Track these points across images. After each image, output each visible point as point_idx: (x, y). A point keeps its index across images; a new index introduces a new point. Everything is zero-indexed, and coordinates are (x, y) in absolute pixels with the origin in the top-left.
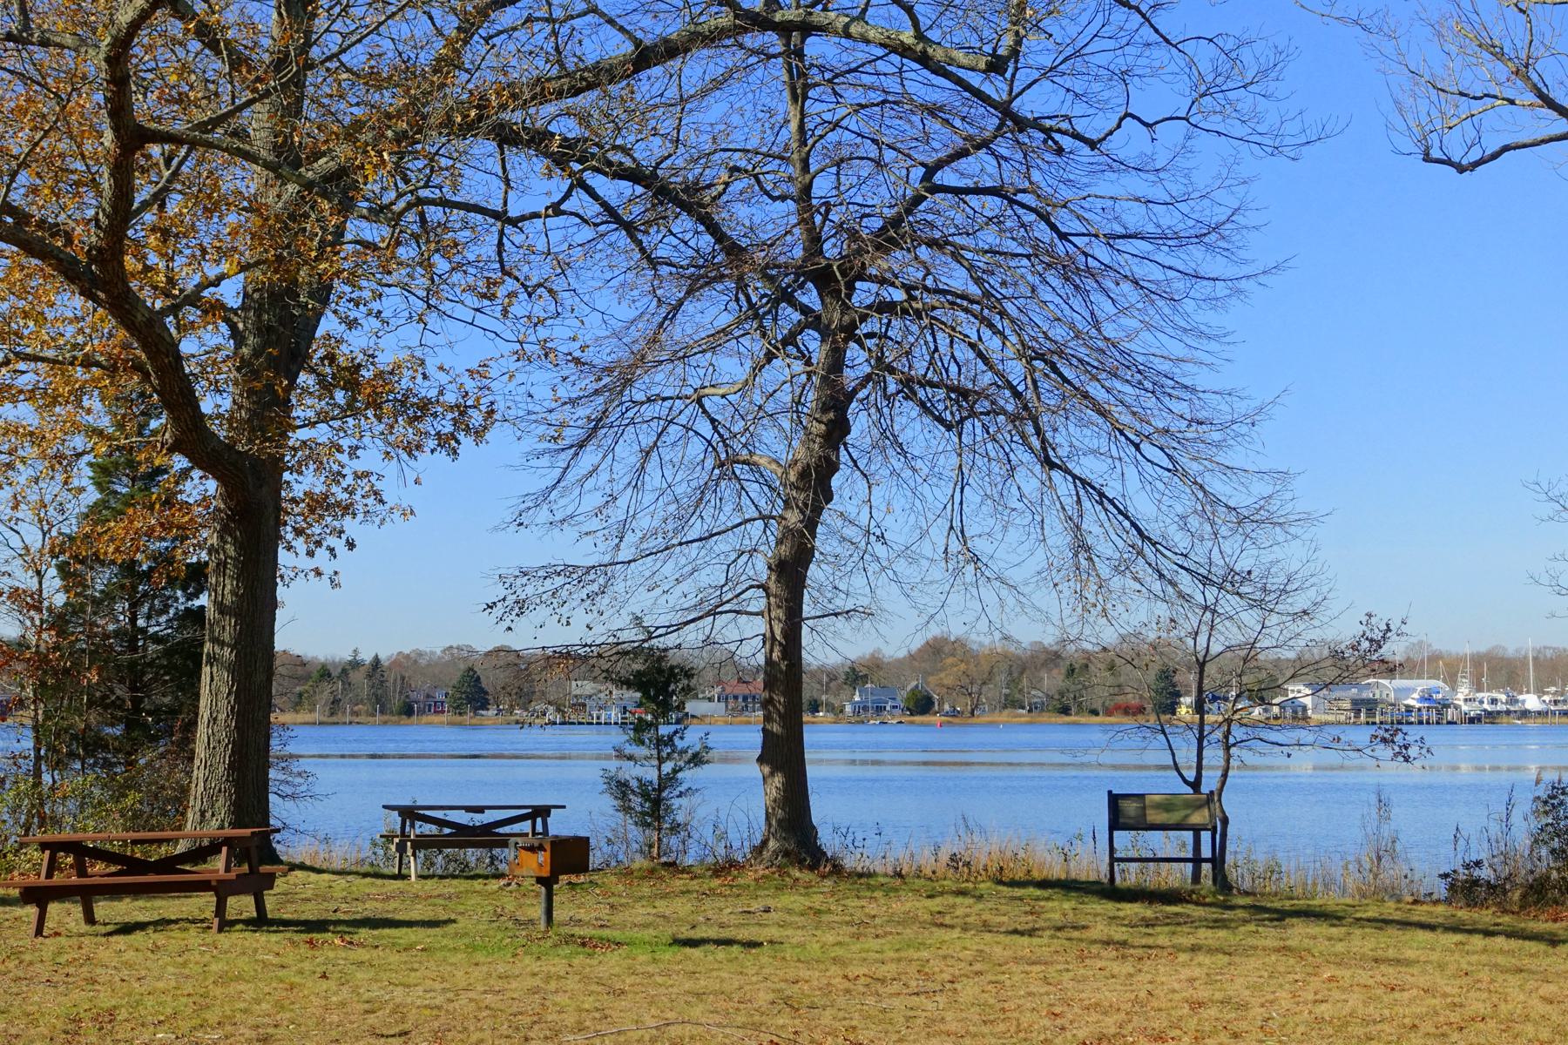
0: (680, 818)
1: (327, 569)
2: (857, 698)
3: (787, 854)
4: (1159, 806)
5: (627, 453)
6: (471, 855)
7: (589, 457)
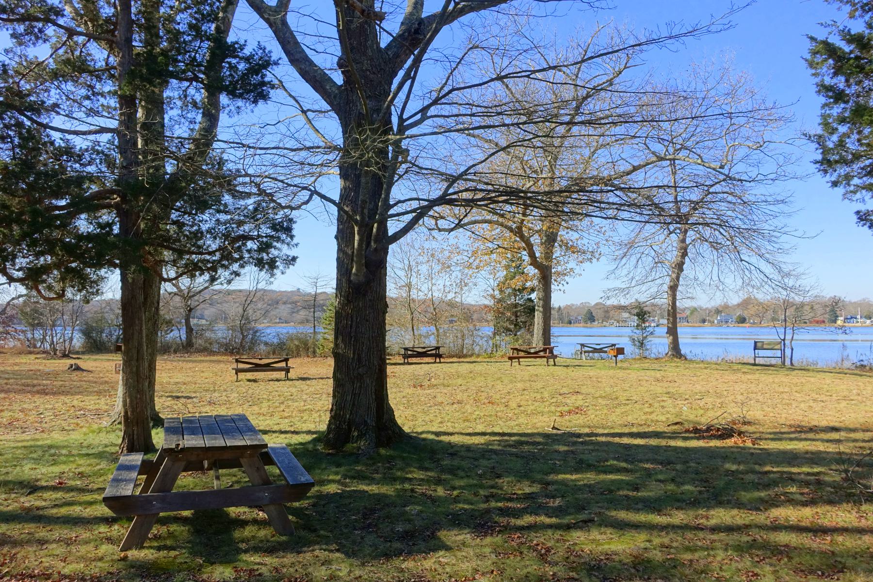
0: (648, 347)
1: (562, 290)
2: (719, 318)
3: (673, 355)
4: (766, 344)
5: (633, 260)
6: (596, 355)
7: (624, 260)
